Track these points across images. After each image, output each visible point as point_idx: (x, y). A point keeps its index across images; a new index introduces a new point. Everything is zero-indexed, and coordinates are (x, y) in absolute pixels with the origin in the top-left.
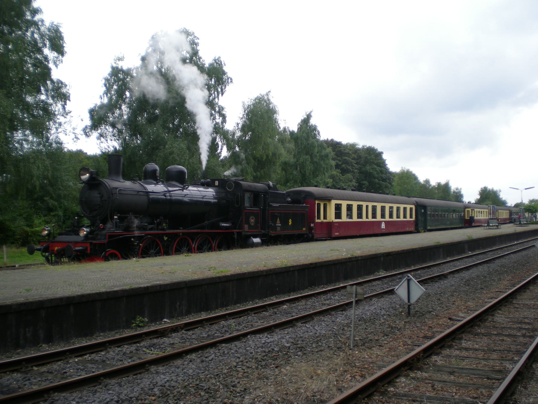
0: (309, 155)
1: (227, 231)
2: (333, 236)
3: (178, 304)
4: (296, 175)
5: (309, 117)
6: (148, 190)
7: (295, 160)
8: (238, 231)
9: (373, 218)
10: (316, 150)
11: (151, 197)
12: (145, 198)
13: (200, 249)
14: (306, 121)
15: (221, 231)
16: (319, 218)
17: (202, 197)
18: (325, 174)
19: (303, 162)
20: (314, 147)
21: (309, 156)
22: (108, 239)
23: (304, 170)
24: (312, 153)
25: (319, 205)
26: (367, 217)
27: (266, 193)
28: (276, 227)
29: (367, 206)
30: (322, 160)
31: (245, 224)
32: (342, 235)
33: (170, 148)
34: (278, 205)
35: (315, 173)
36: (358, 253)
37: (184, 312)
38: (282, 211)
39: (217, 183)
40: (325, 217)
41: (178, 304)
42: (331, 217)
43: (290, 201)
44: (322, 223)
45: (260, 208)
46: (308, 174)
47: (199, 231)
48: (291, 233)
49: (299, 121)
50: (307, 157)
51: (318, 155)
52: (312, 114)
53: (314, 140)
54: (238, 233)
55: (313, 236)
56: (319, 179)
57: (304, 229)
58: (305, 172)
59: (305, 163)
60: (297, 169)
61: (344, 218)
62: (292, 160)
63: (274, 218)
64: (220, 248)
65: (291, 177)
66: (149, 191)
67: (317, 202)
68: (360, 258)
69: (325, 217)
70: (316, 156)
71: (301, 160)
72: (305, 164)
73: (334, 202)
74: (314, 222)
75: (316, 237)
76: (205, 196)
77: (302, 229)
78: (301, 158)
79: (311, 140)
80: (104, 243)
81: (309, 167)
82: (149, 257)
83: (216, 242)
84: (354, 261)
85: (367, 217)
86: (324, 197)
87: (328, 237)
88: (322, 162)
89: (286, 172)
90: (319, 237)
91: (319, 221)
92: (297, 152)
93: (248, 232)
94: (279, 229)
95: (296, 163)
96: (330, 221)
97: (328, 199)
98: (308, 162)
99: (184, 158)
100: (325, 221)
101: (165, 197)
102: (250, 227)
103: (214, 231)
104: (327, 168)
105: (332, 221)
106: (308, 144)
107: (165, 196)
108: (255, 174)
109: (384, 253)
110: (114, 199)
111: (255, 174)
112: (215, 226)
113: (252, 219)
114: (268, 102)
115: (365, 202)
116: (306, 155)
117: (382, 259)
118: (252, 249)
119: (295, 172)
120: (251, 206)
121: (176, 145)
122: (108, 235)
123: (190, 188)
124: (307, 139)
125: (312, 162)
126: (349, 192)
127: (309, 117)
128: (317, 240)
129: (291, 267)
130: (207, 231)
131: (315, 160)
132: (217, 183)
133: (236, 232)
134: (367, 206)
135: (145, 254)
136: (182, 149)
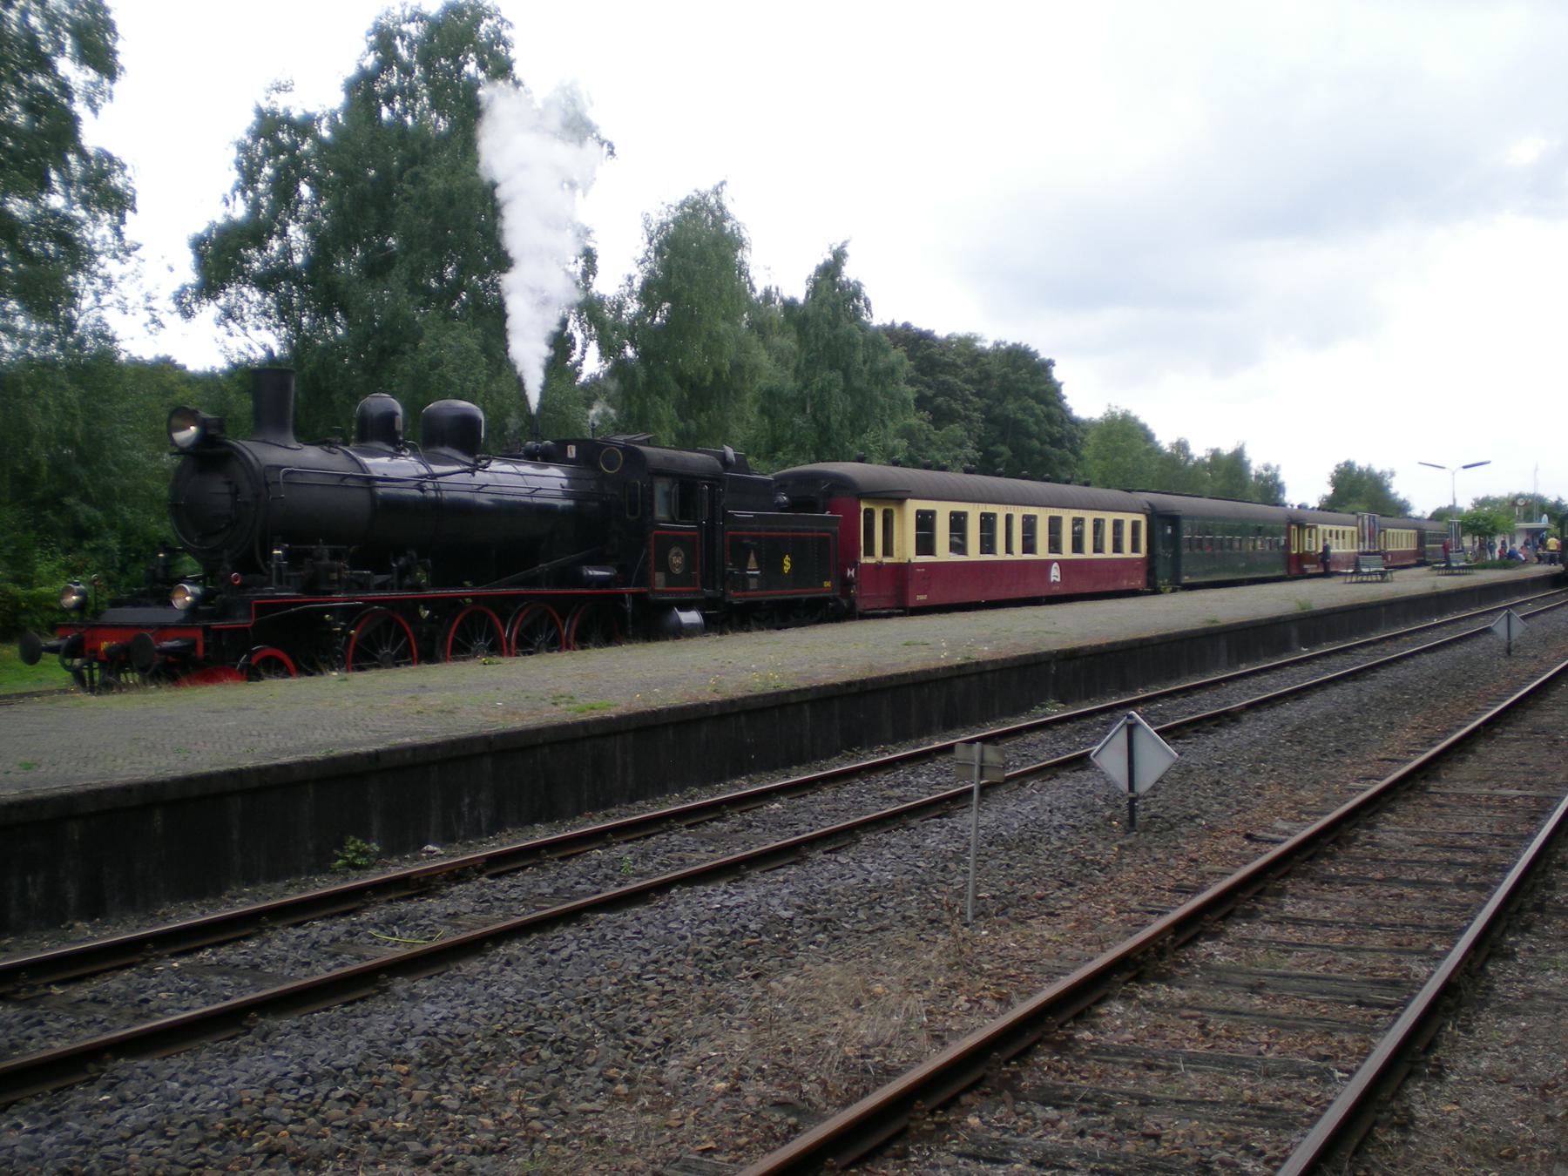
2: (911, 604)
3: (467, 801)
5: (839, 257)
10: (860, 356)
11: (380, 491)
13: (526, 645)
14: (830, 272)
16: (870, 551)
17: (528, 491)
19: (822, 390)
24: (848, 365)
25: (870, 515)
26: (1009, 550)
29: (1009, 518)
32: (938, 602)
34: (750, 514)
36: (984, 652)
39: (572, 451)
40: (887, 551)
41: (467, 801)
43: (785, 503)
44: (878, 567)
46: (835, 426)
49: (811, 271)
51: (866, 369)
52: (848, 250)
55: (853, 605)
56: (868, 437)
58: (828, 418)
60: (804, 410)
62: (791, 385)
63: (740, 552)
65: (789, 434)
67: (863, 506)
68: (989, 667)
69: (887, 551)
71: (817, 384)
73: (913, 506)
74: (854, 563)
75: (860, 607)
77: (822, 586)
81: (840, 405)
82: (378, 667)
85: (1009, 550)
88: (877, 391)
91: (870, 560)
93: (663, 593)
94: (753, 584)
95: (801, 392)
100: (887, 560)
102: (671, 578)
107: (422, 490)
111: (681, 425)
113: (677, 555)
114: (720, 214)
116: (831, 368)
117: (1053, 669)
119: (798, 421)
123: (495, 466)
124: (834, 324)
125: (849, 390)
126: (956, 478)
127: (839, 257)
128: (863, 617)
130: (545, 590)
131: (857, 383)
132: (572, 451)
133: (630, 594)
134: (1009, 518)
136: (469, 350)
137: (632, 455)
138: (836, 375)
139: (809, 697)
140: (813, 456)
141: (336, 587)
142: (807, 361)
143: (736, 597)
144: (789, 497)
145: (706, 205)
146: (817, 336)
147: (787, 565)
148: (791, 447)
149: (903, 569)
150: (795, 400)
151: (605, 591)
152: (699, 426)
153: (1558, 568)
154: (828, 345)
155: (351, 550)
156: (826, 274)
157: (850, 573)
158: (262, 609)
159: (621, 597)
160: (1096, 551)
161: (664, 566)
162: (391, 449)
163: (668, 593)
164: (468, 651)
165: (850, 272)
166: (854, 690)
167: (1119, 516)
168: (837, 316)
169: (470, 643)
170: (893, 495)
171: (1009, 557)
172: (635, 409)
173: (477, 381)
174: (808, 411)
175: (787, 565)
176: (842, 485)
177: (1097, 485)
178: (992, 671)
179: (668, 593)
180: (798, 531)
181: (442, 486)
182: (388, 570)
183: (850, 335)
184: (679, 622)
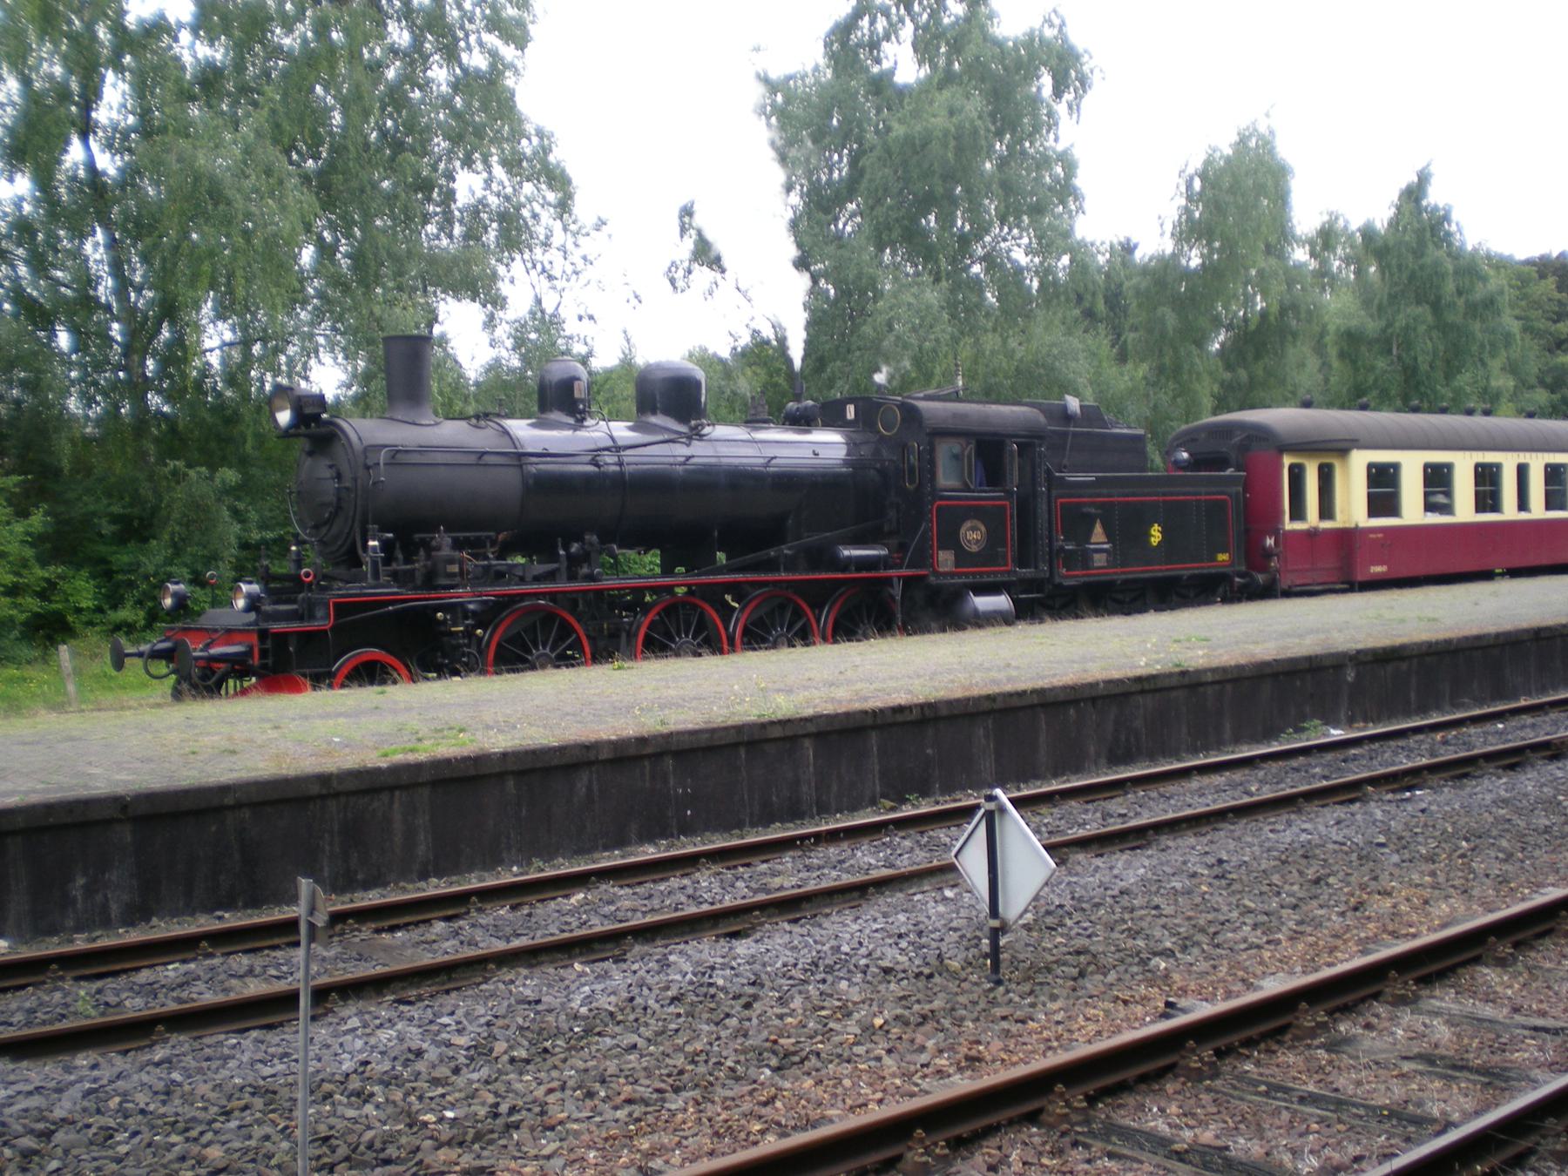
0: (1427, 303)
1: (864, 574)
2: (1360, 578)
3: (81, 881)
4: (1386, 371)
5: (1423, 179)
6: (522, 447)
7: (1383, 323)
8: (905, 572)
9: (1549, 507)
10: (1450, 287)
11: (533, 469)
12: (511, 478)
13: (757, 637)
14: (1413, 195)
15: (840, 575)
16: (1298, 512)
17: (683, 459)
18: (1484, 364)
19: (1407, 327)
20: (1443, 276)
21: (1427, 307)
22: (337, 616)
23: (1412, 353)
24: (1439, 298)
25: (1297, 475)
26: (1523, 505)
27: (1029, 440)
28: (1084, 558)
29: (1522, 471)
30: (1474, 317)
31: (940, 548)
32: (1404, 572)
33: (891, 309)
34: (1090, 477)
35: (1453, 361)
36: (1197, 658)
37: (115, 909)
38: (1115, 499)
39: (851, 412)
40: (1326, 511)
41: (81, 881)
42: (1353, 508)
43: (1185, 461)
44: (1312, 534)
45: (1009, 493)
46: (1424, 368)
47: (750, 577)
48: (1160, 574)
49: (1395, 197)
50: (1420, 310)
51: (1461, 302)
52: (1432, 169)
53: (1441, 253)
54: (908, 582)
55: (1274, 581)
56: (1463, 379)
57: (1223, 557)
58: (1416, 359)
59: (1415, 329)
60: (1390, 351)
61: (1413, 511)
62: (1372, 326)
63: (1078, 524)
64: (845, 630)
65: (1371, 379)
66: (530, 450)
67: (1287, 461)
68: (1209, 677)
69: (1326, 511)
70: (1451, 305)
71: (1401, 321)
72: (1413, 335)
73: (1360, 461)
74: (1275, 531)
75: (1284, 583)
76: (772, 458)
77: (1213, 559)
78: (1401, 316)
79: (1434, 254)
80: (325, 631)
81: (1427, 347)
82: (533, 668)
83: (828, 612)
84: (1172, 688)
85: (1523, 505)
86: (1330, 441)
87: (1343, 583)
88: (1476, 326)
89: (1354, 362)
90: (1298, 582)
91: (1298, 526)
92: (1386, 297)
93: (952, 575)
94: (1099, 560)
95: (1384, 331)
96: (1347, 525)
97: (1338, 447)
98: (1422, 328)
99: (933, 337)
100: (1327, 525)
101: (596, 469)
102: (962, 556)
103: (824, 575)
104: (1492, 345)
105: (1353, 525)
106: (1422, 268)
107: (597, 465)
108: (1227, 376)
109: (1359, 652)
110: (374, 483)
111: (1227, 376)
112: (822, 557)
113: (974, 529)
114: (1267, 144)
115: (1509, 455)
116: (1418, 303)
117: (1350, 676)
118: (960, 635)
119: (1381, 364)
120: (966, 484)
121: (912, 300)
122: (335, 603)
123: (721, 431)
124: (1419, 252)
125: (1443, 327)
126: (1506, 422)
127: (1423, 179)
128: (1288, 594)
129: (772, 723)
130: (783, 576)
131: (1450, 317)
132: (851, 412)
133: (899, 577)
134: (1522, 471)
135: (658, 645)
136: (929, 307)
137: (911, 414)
138: (1424, 311)
139: (811, 728)
140: (1399, 403)
141: (457, 580)
142: (1390, 294)
143: (1069, 577)
144: (1191, 455)
145: (1255, 130)
146: (1400, 267)
147: (1156, 535)
148: (1375, 393)
149: (1347, 537)
150: (1377, 340)
151: (864, 574)
152: (1251, 378)
153: (417, 536)
154: (1412, 277)
155: (501, 537)
156: (1409, 198)
157: (1270, 542)
158: (342, 609)
159: (888, 581)
160: (1480, 507)
161: (950, 540)
162: (571, 421)
163: (959, 575)
164: (764, 640)
165: (1435, 196)
166: (999, 705)
167: (1523, 457)
168: (1421, 243)
169: (857, 626)
170: (1330, 446)
171: (1524, 516)
172: (1167, 360)
173: (937, 340)
174: (1395, 351)
175: (1156, 535)
176: (1260, 434)
177: (1319, 406)
178: (1213, 683)
179: (959, 575)
180: (1172, 494)
181: (626, 460)
182: (554, 557)
183: (1437, 264)
184: (976, 610)
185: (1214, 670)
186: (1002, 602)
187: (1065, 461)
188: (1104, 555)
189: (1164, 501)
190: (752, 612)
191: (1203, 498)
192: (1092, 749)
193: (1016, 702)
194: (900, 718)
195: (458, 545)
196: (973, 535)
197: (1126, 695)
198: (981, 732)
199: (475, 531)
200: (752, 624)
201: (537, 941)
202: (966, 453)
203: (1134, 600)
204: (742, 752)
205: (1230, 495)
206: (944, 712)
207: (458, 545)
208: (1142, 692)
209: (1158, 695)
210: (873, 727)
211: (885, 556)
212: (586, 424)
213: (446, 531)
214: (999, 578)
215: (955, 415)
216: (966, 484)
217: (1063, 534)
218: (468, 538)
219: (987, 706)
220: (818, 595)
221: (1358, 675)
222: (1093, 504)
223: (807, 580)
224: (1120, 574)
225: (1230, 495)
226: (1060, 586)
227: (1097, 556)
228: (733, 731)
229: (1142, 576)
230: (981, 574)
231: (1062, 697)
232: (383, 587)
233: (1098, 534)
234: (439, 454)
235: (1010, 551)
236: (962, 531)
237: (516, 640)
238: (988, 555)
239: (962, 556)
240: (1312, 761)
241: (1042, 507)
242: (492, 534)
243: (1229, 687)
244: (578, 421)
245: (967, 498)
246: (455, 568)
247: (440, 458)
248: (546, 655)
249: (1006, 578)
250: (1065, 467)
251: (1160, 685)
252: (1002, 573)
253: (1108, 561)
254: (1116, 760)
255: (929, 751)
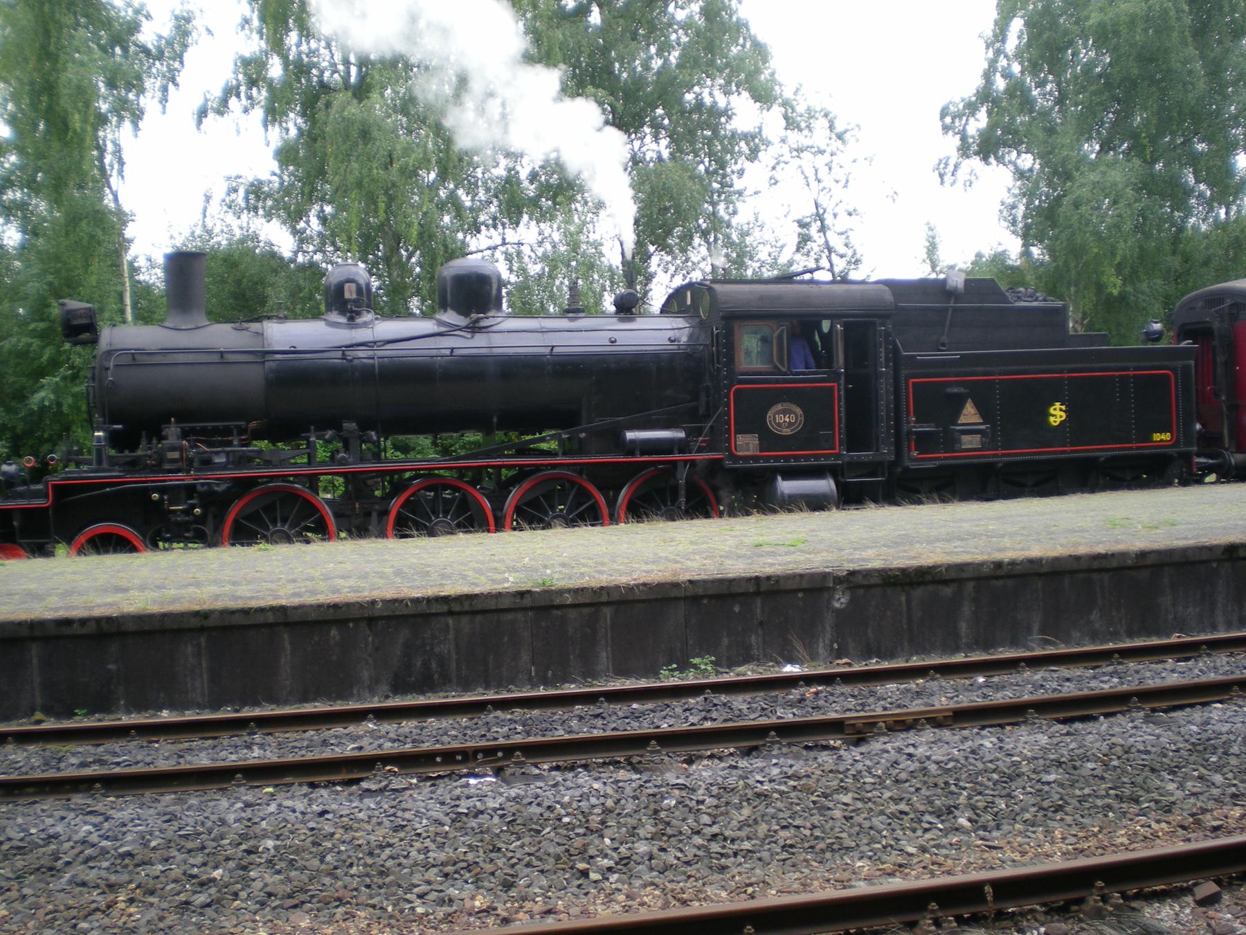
28: (950, 441)
31: (737, 432)
34: (954, 355)
93: (755, 458)
117: (840, 601)
162: (343, 320)
179: (767, 459)
185: (577, 591)
186: (825, 485)
187: (944, 339)
188: (978, 437)
189: (1070, 379)
190: (529, 490)
191: (1131, 373)
192: (365, 675)
193: (237, 620)
194: (66, 631)
195: (185, 435)
196: (784, 419)
197: (426, 617)
198: (190, 649)
199: (222, 421)
200: (525, 504)
201: (609, 733)
202: (776, 334)
203: (1036, 484)
204: (759, 602)
205: (1174, 370)
206: (131, 627)
207: (185, 435)
208: (451, 613)
209: (479, 618)
210: (607, 604)
211: (680, 440)
212: (359, 320)
213: (177, 422)
214: (823, 462)
215: (762, 298)
216: (776, 367)
217: (915, 414)
218: (217, 427)
219: (195, 622)
220: (610, 479)
221: (852, 601)
222: (957, 384)
223: (589, 463)
224: (1001, 456)
225: (1174, 370)
226: (907, 469)
227: (965, 438)
228: (93, 624)
229: (1036, 457)
230: (796, 458)
231: (313, 616)
232: (103, 471)
233: (970, 414)
234: (181, 355)
235: (839, 433)
236: (770, 414)
237: (254, 517)
238: (807, 437)
239: (769, 439)
240: (934, 685)
241: (884, 388)
242: (242, 423)
243: (607, 612)
244: (351, 319)
245: (777, 381)
246: (176, 455)
247: (181, 358)
248: (440, 522)
249: (831, 462)
250: (943, 345)
251: (479, 606)
252: (827, 456)
253: (982, 443)
254: (399, 687)
255: (112, 667)
